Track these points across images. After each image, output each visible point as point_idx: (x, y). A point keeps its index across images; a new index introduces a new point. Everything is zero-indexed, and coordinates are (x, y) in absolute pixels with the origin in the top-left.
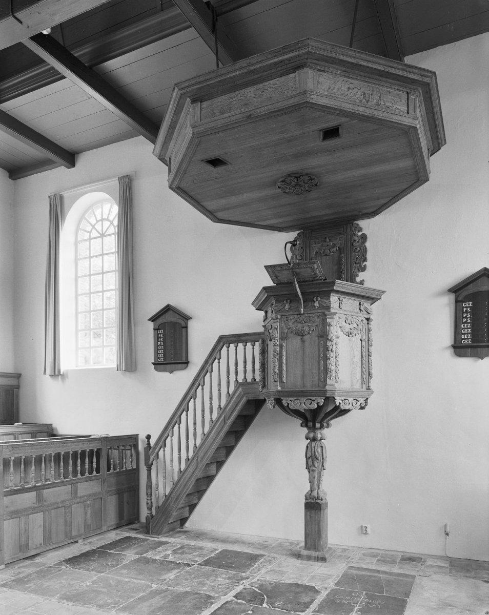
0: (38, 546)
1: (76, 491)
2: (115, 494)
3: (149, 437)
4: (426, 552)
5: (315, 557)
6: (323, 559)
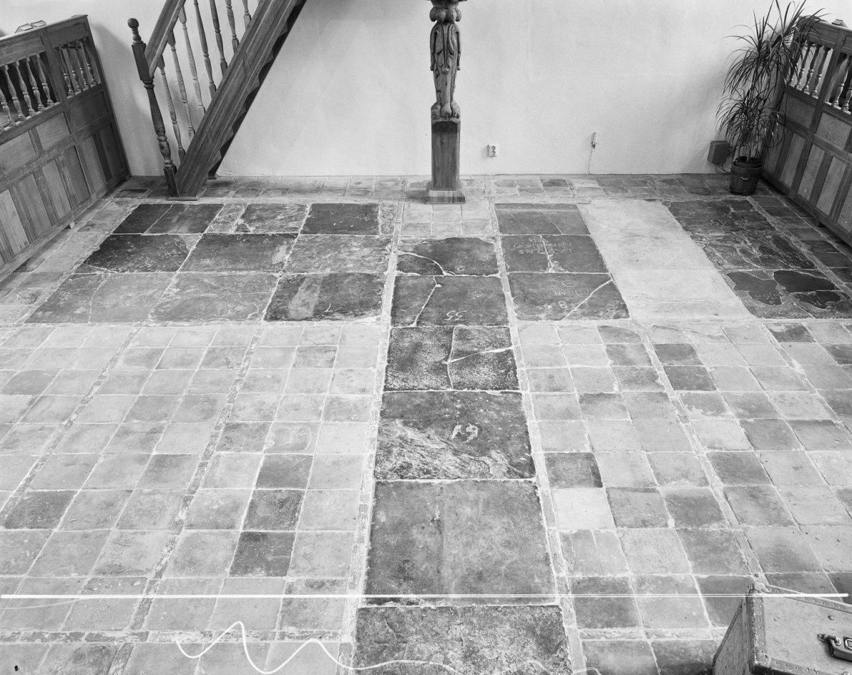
0: (24, 246)
1: (37, 142)
2: (90, 136)
3: (134, 24)
4: (567, 172)
5: (449, 198)
6: (461, 200)
